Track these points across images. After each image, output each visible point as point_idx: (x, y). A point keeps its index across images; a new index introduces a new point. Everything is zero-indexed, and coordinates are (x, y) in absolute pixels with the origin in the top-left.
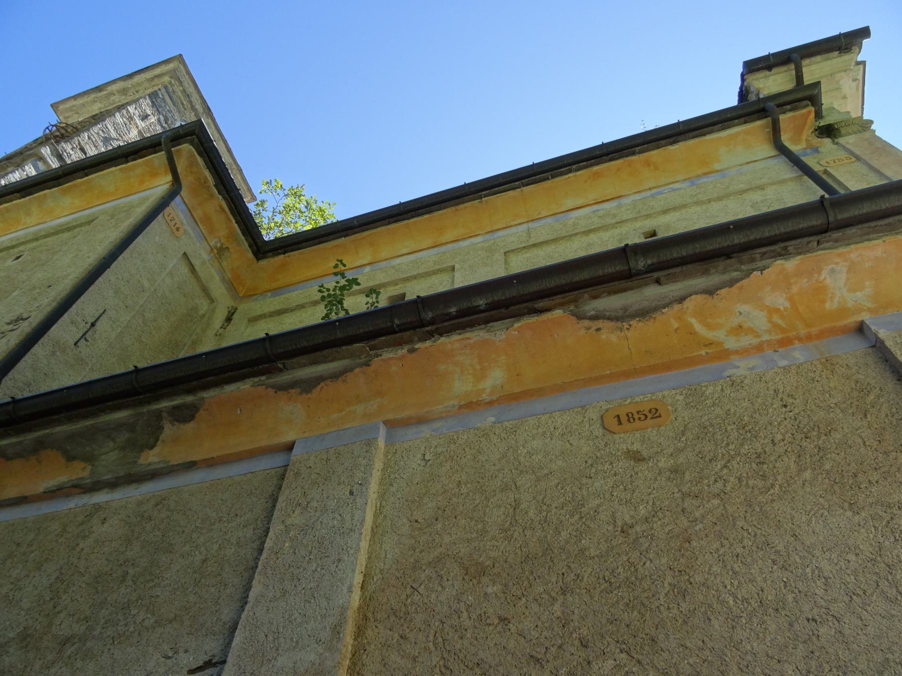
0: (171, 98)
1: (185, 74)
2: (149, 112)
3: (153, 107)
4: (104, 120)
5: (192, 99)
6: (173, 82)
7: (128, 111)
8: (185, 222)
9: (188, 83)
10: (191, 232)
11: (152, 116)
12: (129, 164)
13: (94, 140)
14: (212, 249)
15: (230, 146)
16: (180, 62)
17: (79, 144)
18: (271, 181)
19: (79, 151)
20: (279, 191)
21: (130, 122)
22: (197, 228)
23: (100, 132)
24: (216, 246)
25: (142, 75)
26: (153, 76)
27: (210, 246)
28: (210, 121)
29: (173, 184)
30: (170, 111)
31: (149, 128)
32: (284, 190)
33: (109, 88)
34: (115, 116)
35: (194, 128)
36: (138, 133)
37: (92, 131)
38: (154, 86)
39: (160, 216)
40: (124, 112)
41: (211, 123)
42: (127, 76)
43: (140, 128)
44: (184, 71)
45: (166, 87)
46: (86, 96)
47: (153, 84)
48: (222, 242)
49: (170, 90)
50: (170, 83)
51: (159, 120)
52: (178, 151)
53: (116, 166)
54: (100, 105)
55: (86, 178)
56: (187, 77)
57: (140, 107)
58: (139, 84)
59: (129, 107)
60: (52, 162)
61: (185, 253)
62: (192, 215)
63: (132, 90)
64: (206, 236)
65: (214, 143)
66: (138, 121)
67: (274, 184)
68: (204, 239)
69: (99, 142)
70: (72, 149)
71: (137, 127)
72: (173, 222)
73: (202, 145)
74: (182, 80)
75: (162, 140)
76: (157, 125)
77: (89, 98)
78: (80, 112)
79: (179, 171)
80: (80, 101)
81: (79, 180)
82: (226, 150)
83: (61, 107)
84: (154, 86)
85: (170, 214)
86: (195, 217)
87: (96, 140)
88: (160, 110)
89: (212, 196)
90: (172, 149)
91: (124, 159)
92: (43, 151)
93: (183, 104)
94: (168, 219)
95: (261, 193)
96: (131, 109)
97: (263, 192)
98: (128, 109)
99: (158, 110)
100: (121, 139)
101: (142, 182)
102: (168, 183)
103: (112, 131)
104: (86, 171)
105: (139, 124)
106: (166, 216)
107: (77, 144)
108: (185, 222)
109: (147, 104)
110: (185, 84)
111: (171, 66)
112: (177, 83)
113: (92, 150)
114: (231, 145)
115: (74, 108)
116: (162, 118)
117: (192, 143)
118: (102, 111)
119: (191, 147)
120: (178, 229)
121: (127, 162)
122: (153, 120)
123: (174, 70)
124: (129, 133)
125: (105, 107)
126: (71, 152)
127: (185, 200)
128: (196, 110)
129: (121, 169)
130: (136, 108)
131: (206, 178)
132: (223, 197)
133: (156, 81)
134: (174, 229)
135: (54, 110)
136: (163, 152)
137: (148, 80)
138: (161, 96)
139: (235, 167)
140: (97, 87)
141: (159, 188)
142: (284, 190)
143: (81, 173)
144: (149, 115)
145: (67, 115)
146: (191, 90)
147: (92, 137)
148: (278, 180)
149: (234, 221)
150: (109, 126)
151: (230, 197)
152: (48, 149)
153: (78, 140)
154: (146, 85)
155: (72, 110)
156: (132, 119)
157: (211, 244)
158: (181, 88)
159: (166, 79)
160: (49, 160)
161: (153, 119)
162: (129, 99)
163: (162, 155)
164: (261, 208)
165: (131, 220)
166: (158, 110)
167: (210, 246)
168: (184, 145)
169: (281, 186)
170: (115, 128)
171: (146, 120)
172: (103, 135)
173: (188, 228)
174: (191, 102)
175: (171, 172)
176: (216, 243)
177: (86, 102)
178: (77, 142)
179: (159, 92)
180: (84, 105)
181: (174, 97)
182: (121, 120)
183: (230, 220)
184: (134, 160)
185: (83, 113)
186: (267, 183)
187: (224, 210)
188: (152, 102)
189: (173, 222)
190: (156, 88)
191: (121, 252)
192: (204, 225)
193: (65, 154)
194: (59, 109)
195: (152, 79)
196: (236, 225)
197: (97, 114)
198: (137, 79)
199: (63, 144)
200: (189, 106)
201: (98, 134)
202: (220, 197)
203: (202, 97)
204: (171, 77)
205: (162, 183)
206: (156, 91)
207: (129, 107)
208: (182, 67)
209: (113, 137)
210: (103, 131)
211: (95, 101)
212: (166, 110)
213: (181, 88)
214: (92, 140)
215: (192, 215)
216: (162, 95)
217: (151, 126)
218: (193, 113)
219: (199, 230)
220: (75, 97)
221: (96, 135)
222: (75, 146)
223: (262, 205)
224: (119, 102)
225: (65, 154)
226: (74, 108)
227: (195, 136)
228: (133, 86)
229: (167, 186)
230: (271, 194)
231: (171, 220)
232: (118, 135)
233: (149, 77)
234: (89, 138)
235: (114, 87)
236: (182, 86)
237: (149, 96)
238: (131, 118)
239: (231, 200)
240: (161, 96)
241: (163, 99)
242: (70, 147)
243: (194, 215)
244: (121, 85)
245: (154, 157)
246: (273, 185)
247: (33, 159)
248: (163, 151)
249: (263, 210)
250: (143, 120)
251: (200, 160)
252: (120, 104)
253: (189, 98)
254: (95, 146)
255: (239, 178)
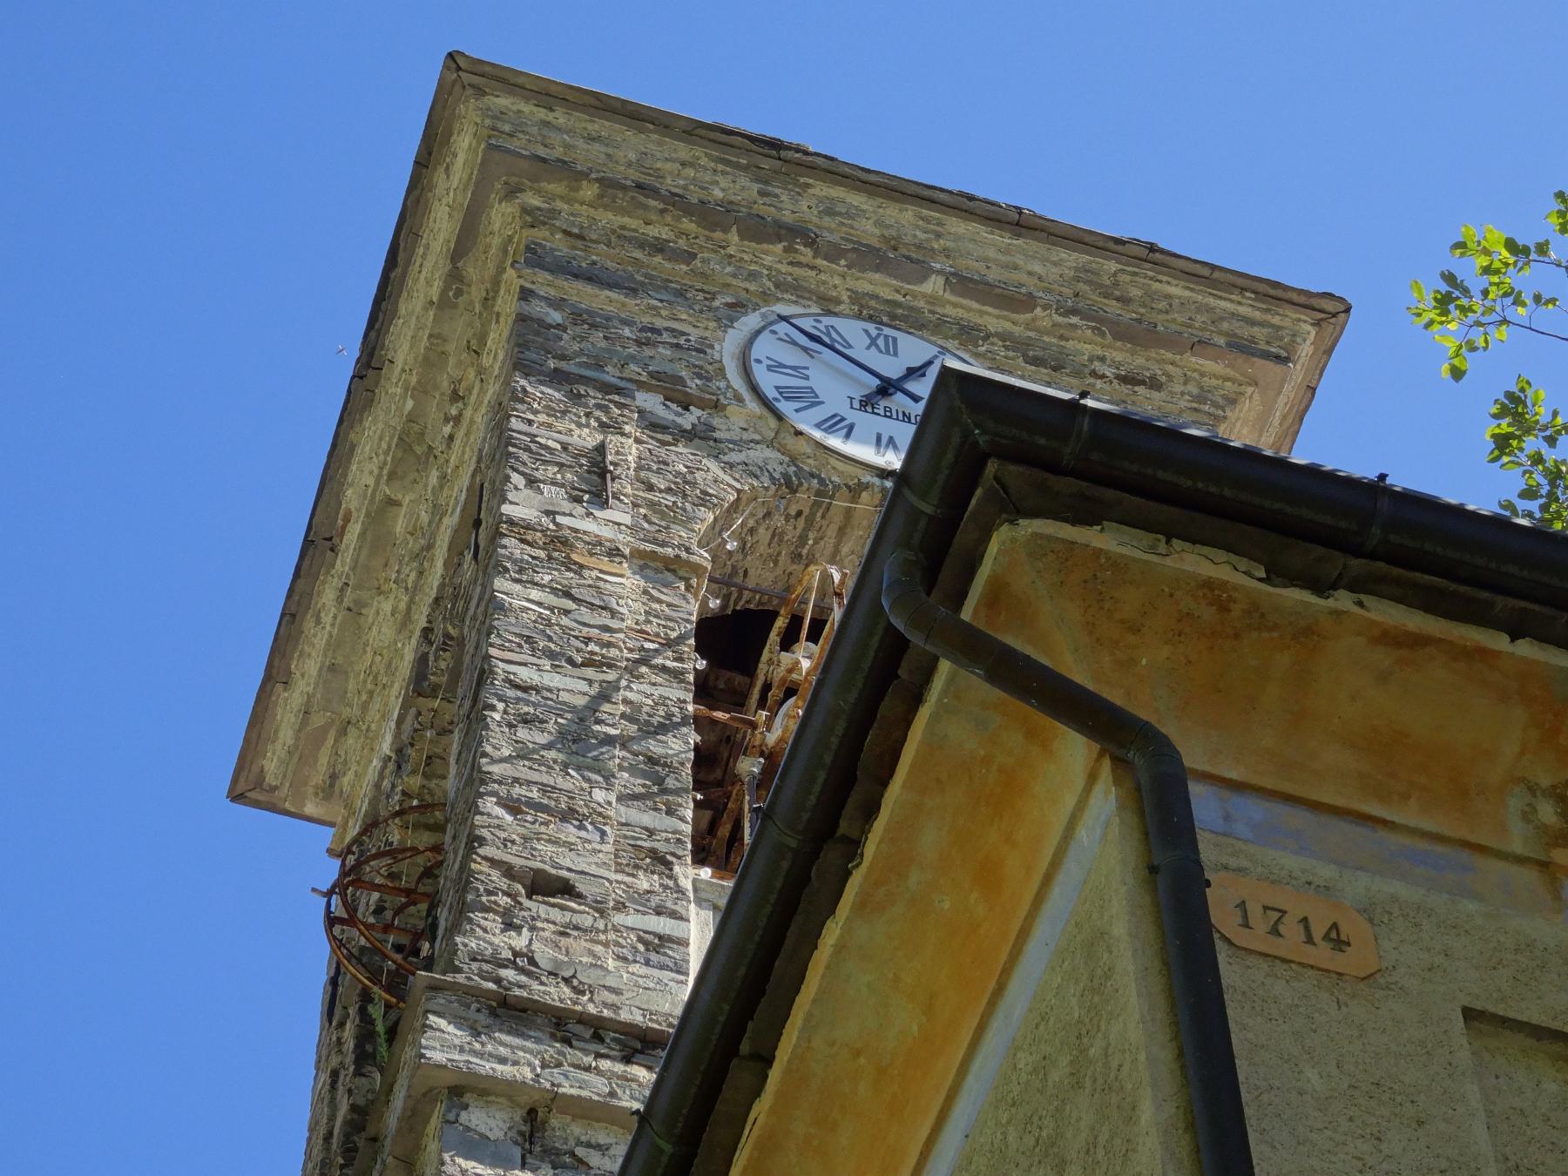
0: (590, 277)
1: (542, 114)
2: (587, 438)
3: (576, 398)
4: (484, 675)
5: (669, 184)
6: (535, 201)
7: (521, 528)
8: (1325, 872)
9: (591, 139)
10: (1397, 888)
11: (613, 440)
12: (870, 849)
13: (535, 794)
14: (1544, 866)
15: (1003, 199)
16: (480, 92)
17: (508, 871)
18: (1449, 278)
19: (535, 906)
20: (1528, 279)
21: (568, 564)
22: (1394, 840)
23: (522, 733)
24: (1543, 829)
25: (403, 308)
26: (444, 267)
27: (1520, 860)
28: (821, 189)
29: (1119, 762)
30: (649, 336)
31: (652, 505)
32: (1542, 248)
33: (352, 498)
34: (501, 607)
35: (956, 440)
36: (641, 570)
37: (496, 769)
38: (487, 301)
39: (1230, 971)
40: (512, 546)
41: (837, 192)
42: (358, 376)
43: (625, 541)
44: (527, 108)
45: (535, 257)
46: (309, 624)
47: (476, 293)
48: (1545, 781)
49: (559, 245)
50: (533, 219)
51: (653, 426)
52: (996, 596)
53: (832, 911)
54: (387, 607)
55: (775, 1074)
56: (560, 117)
57: (541, 454)
58: (433, 359)
59: (506, 509)
60: (503, 1060)
61: (1471, 1015)
62: (1316, 807)
63: (433, 413)
64: (1463, 833)
65: (1090, 402)
66: (587, 525)
67: (1470, 270)
68: (1465, 856)
69: (561, 782)
70: (509, 926)
71: (614, 553)
72: (1291, 928)
73: (1053, 467)
74: (558, 152)
75: (898, 623)
76: (662, 452)
77: (327, 619)
78: (346, 712)
79: (1080, 675)
80: (308, 668)
81: (761, 1109)
82: (1002, 239)
83: (272, 765)
84: (487, 301)
85: (1242, 905)
86: (1340, 802)
87: (545, 789)
88: (611, 375)
89: (1306, 634)
90: (966, 615)
91: (831, 855)
92: (437, 1056)
93: (659, 247)
94: (1257, 939)
95: (1457, 374)
96: (521, 505)
97: (1468, 363)
98: (511, 522)
99: (607, 388)
100: (611, 676)
101: (989, 877)
102: (1092, 778)
103: (553, 680)
104: (745, 1047)
105: (607, 532)
106: (1241, 937)
107: (503, 883)
108: (1325, 872)
109: (550, 411)
110: (587, 154)
111: (464, 146)
112: (552, 187)
113: (570, 846)
114: (1005, 194)
115: (318, 720)
116: (650, 401)
117: (1016, 510)
118: (423, 623)
119: (1030, 527)
120: (1338, 942)
121: (853, 847)
122: (632, 452)
123: (494, 149)
124: (614, 614)
125: (414, 592)
126: (520, 941)
127: (1233, 775)
128: (728, 207)
129: (861, 906)
130: (532, 482)
131: (1209, 584)
132: (1352, 589)
133: (476, 272)
134: (1322, 954)
135: (257, 804)
136: (945, 666)
137: (444, 305)
138: (556, 317)
139: (1113, 266)
140: (308, 543)
141: (1082, 834)
142: (1542, 248)
143: (739, 1075)
144: (601, 449)
145: (319, 775)
146: (631, 145)
147: (517, 791)
148: (1470, 232)
149: (1499, 642)
150: (525, 674)
151: (1373, 556)
152: (442, 1023)
153: (493, 863)
154: (459, 329)
155: (318, 739)
156: (565, 542)
157: (1517, 846)
158: (589, 191)
159: (501, 217)
160: (487, 1067)
161: (628, 450)
162: (463, 458)
163: (951, 680)
164: (1532, 443)
165: (1147, 1113)
166: (607, 388)
167: (1520, 860)
168: (993, 548)
169: (1511, 245)
170: (551, 655)
171: (612, 487)
172: (543, 739)
173: (1358, 885)
174: (676, 202)
175: (1058, 716)
176: (1528, 815)
177: (333, 645)
178: (495, 875)
179: (538, 308)
180: (332, 668)
181: (602, 257)
182: (535, 594)
183: (1483, 653)
184: (871, 810)
185: (365, 707)
186: (1444, 302)
187: (1418, 641)
188: (558, 378)
189: (1291, 928)
190: (507, 305)
191: (963, 1079)
192: (1406, 797)
193: (509, 974)
194: (270, 780)
195: (455, 278)
196: (1526, 649)
197: (422, 661)
198: (403, 347)
199: (467, 942)
200: (688, 225)
201: (523, 753)
202: (1343, 600)
203: (694, 131)
204: (512, 192)
205: (1070, 801)
206: (522, 319)
207: (506, 509)
208: (503, 102)
209: (581, 701)
210: (526, 721)
211: (355, 611)
212: (633, 349)
213: (589, 191)
214: (531, 804)
215: (1316, 807)
216: (557, 304)
217: (650, 488)
218: (734, 237)
219: (1406, 841)
220: (276, 675)
221: (522, 770)
222: (504, 900)
223: (1524, 425)
224: (438, 512)
225: (509, 974)
226: (318, 720)
227: (992, 467)
228: (422, 391)
229: (1106, 801)
230: (1502, 333)
231: (1275, 931)
232: (590, 672)
233: (437, 285)
234: (514, 807)
235: (363, 474)
236: (585, 175)
237: (521, 366)
238: (559, 543)
239: (1392, 561)
240: (556, 317)
241: (577, 316)
242: (493, 923)
243: (1327, 798)
244: (374, 435)
245: (935, 718)
246: (1475, 283)
247: (434, 1122)
248: (936, 659)
249: (1551, 441)
250: (600, 498)
251: (1106, 539)
252: (450, 521)
253: (653, 192)
254: (568, 815)
255: (1177, 290)
